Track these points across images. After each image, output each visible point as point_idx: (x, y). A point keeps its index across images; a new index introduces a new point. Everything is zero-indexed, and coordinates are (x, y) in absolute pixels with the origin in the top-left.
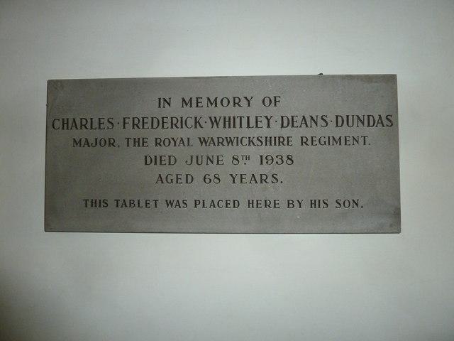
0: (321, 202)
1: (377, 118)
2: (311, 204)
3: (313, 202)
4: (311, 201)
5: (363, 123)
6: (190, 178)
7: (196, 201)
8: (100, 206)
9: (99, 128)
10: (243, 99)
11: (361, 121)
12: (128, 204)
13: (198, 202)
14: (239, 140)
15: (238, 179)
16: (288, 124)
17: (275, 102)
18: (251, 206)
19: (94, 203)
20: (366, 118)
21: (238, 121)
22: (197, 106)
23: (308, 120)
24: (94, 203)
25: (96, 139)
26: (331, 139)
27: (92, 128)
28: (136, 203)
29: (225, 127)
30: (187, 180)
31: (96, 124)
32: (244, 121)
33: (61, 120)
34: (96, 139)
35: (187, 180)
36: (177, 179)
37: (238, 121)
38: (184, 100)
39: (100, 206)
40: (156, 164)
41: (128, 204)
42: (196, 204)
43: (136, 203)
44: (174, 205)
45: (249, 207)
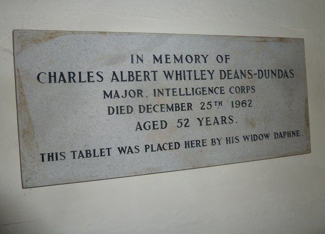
0: (234, 138)
1: (284, 72)
2: (227, 140)
3: (187, 143)
4: (186, 142)
5: (275, 75)
6: (164, 124)
7: (146, 146)
8: (57, 159)
9: (89, 81)
10: (201, 57)
11: (274, 73)
12: (85, 155)
13: (147, 147)
14: (194, 90)
15: (204, 122)
16: (282, 76)
17: (226, 59)
18: (187, 147)
19: (51, 157)
20: (277, 71)
21: (187, 74)
22: (167, 62)
23: (239, 74)
24: (51, 157)
25: (193, 89)
26: (157, 91)
27: (80, 81)
28: (92, 153)
29: (177, 79)
30: (162, 126)
31: (84, 77)
32: (192, 74)
33: (48, 74)
34: (193, 89)
35: (162, 126)
36: (154, 125)
37: (187, 74)
38: (155, 57)
39: (57, 159)
40: (117, 113)
41: (85, 155)
42: (146, 149)
43: (92, 153)
44: (127, 152)
45: (227, 143)
